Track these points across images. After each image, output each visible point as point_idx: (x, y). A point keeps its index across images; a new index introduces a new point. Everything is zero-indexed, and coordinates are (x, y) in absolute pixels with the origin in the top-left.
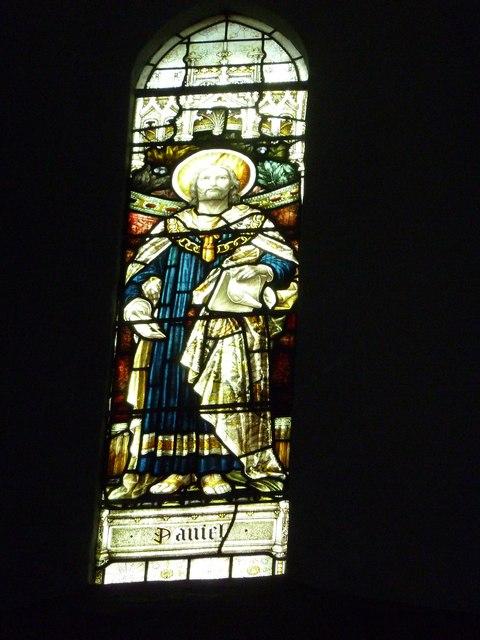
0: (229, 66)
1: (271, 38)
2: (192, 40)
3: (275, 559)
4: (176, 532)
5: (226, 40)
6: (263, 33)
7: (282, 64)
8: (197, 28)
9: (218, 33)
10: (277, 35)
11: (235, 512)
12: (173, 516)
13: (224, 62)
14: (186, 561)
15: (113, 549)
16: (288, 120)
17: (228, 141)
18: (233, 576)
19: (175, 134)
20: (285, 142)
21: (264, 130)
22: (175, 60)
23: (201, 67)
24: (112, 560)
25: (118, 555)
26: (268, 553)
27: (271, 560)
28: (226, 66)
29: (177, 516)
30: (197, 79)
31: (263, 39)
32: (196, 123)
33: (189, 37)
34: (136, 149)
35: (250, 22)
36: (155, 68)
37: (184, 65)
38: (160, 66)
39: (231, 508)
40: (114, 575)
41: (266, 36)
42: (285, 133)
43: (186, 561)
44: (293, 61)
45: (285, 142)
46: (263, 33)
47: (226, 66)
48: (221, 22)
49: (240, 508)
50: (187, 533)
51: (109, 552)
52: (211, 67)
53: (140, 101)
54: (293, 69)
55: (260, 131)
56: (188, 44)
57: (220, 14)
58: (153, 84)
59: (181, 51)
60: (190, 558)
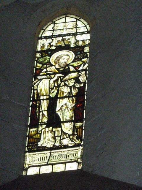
0: (66, 29)
1: (79, 20)
2: (67, 16)
3: (79, 163)
4: (70, 157)
5: (66, 22)
6: (77, 19)
7: (82, 26)
8: (58, 19)
9: (63, 20)
10: (81, 20)
11: (51, 153)
12: (74, 150)
13: (65, 28)
14: (39, 167)
15: (30, 163)
16: (84, 41)
17: (67, 47)
18: (66, 170)
19: (50, 48)
20: (83, 47)
21: (77, 44)
22: (50, 27)
23: (58, 30)
24: (30, 167)
25: (31, 165)
26: (76, 161)
27: (77, 164)
28: (65, 29)
29: (76, 150)
30: (56, 33)
31: (76, 21)
32: (57, 44)
33: (54, 22)
34: (45, 97)
35: (72, 16)
36: (44, 31)
37: (53, 30)
38: (46, 30)
39: (50, 151)
40: (31, 172)
41: (77, 20)
42: (83, 45)
43: (39, 167)
44: (86, 26)
45: (83, 47)
46: (77, 19)
47: (65, 29)
48: (64, 17)
49: (52, 151)
50: (42, 159)
51: (28, 164)
52: (61, 29)
53: (40, 41)
54: (86, 28)
55: (76, 44)
56: (54, 24)
57: (64, 15)
58: (44, 35)
59: (52, 25)
60: (40, 166)
